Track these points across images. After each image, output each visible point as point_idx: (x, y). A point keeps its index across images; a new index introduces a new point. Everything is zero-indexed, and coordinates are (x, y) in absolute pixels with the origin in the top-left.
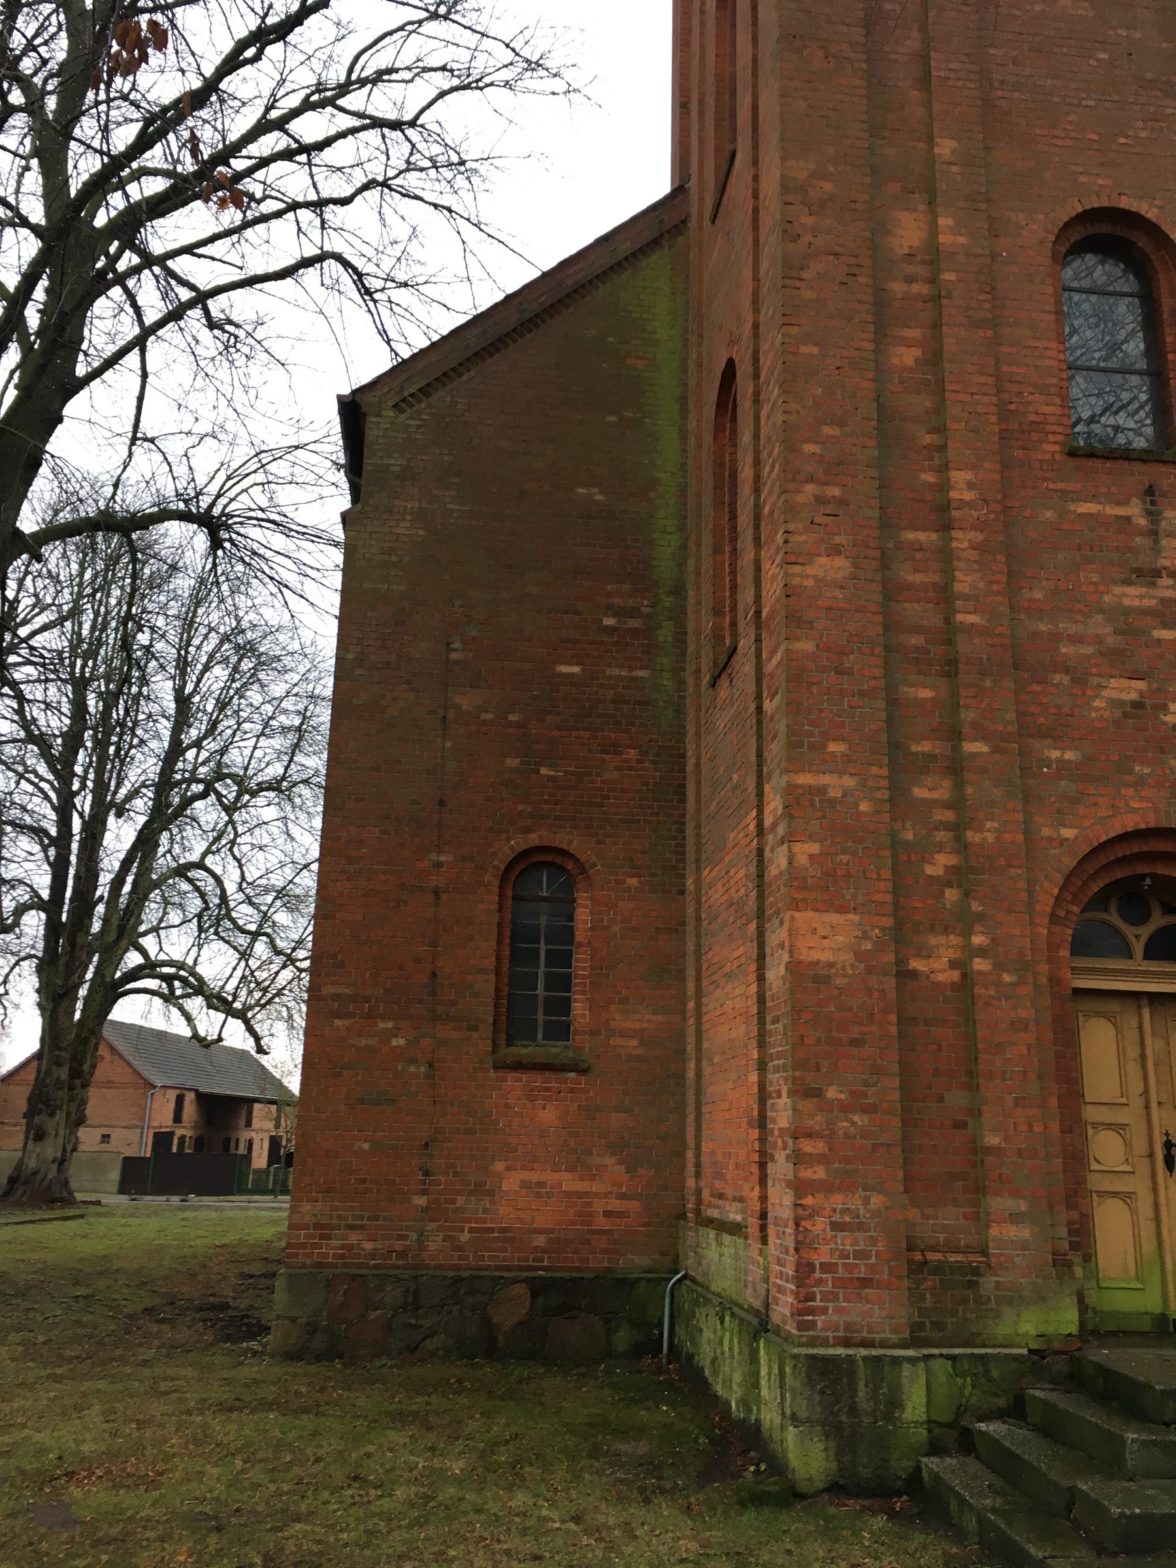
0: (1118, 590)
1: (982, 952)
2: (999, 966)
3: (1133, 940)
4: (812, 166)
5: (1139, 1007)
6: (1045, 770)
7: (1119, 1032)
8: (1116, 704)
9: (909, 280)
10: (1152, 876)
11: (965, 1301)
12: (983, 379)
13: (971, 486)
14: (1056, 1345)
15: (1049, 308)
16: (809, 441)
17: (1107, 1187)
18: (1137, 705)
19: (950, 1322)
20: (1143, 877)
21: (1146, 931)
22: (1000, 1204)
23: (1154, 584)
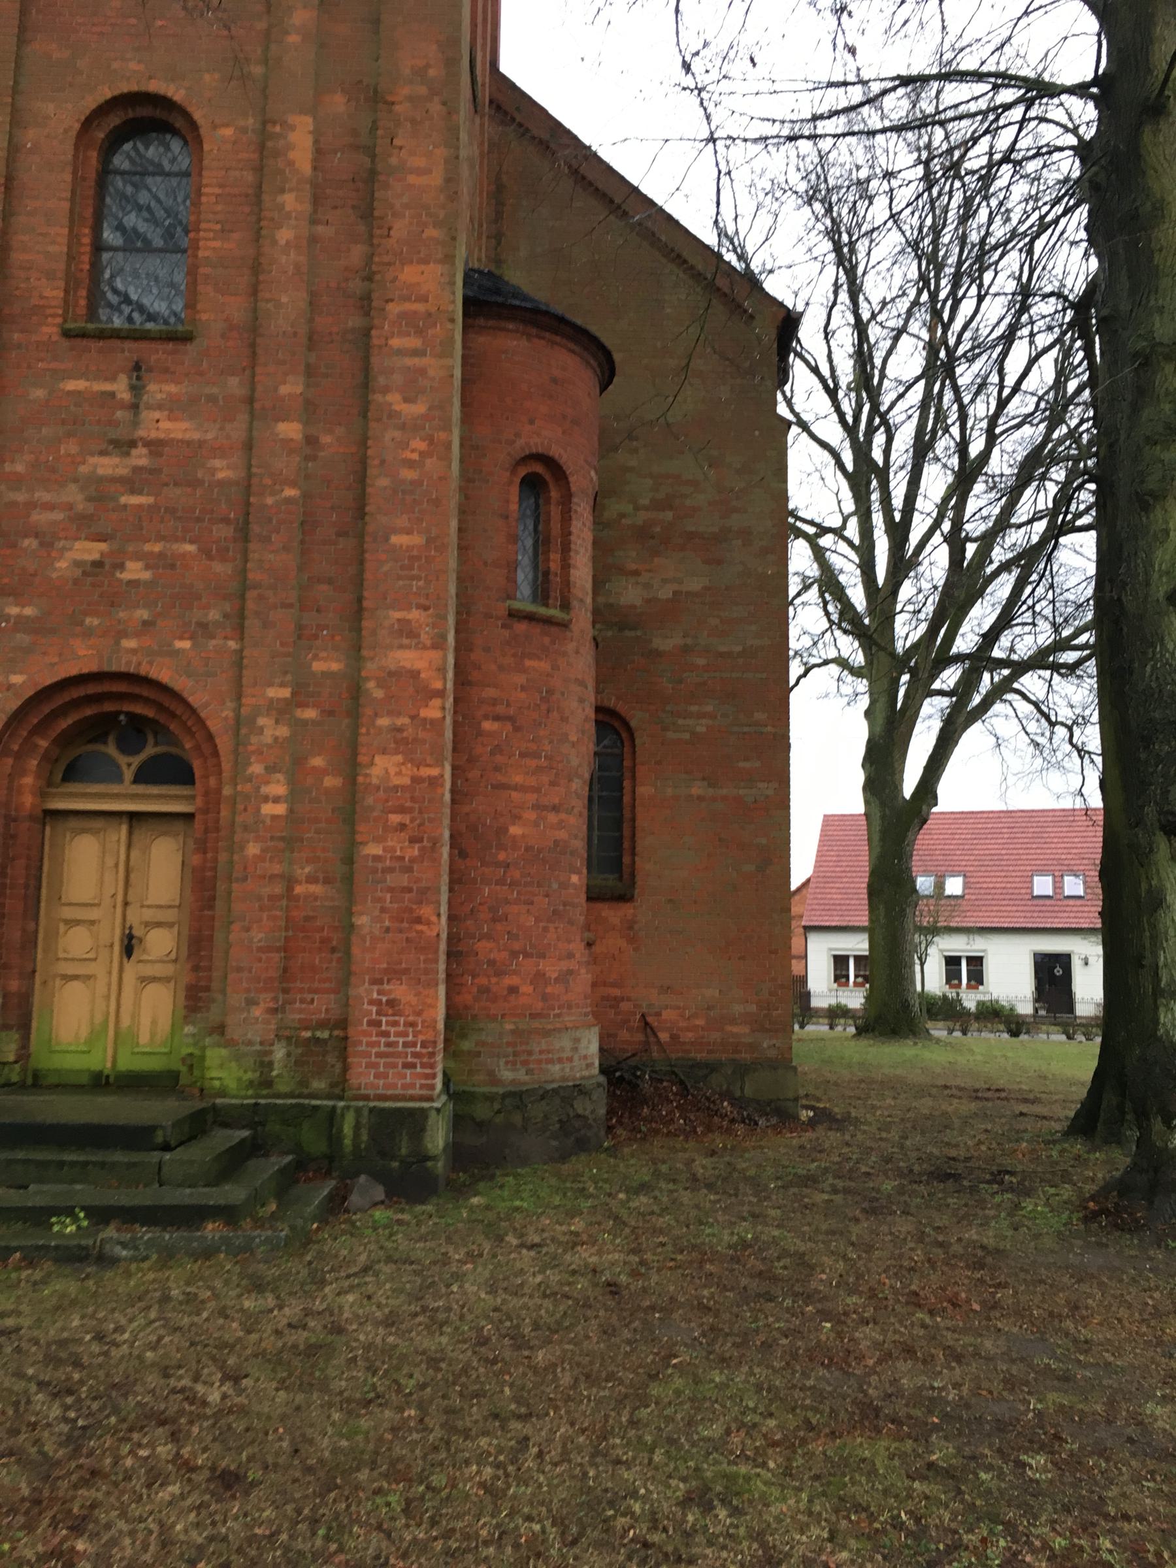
0: (93, 460)
3: (124, 768)
8: (77, 564)
10: (127, 714)
15: (64, 195)
17: (70, 972)
18: (97, 564)
20: (119, 713)
21: (136, 761)
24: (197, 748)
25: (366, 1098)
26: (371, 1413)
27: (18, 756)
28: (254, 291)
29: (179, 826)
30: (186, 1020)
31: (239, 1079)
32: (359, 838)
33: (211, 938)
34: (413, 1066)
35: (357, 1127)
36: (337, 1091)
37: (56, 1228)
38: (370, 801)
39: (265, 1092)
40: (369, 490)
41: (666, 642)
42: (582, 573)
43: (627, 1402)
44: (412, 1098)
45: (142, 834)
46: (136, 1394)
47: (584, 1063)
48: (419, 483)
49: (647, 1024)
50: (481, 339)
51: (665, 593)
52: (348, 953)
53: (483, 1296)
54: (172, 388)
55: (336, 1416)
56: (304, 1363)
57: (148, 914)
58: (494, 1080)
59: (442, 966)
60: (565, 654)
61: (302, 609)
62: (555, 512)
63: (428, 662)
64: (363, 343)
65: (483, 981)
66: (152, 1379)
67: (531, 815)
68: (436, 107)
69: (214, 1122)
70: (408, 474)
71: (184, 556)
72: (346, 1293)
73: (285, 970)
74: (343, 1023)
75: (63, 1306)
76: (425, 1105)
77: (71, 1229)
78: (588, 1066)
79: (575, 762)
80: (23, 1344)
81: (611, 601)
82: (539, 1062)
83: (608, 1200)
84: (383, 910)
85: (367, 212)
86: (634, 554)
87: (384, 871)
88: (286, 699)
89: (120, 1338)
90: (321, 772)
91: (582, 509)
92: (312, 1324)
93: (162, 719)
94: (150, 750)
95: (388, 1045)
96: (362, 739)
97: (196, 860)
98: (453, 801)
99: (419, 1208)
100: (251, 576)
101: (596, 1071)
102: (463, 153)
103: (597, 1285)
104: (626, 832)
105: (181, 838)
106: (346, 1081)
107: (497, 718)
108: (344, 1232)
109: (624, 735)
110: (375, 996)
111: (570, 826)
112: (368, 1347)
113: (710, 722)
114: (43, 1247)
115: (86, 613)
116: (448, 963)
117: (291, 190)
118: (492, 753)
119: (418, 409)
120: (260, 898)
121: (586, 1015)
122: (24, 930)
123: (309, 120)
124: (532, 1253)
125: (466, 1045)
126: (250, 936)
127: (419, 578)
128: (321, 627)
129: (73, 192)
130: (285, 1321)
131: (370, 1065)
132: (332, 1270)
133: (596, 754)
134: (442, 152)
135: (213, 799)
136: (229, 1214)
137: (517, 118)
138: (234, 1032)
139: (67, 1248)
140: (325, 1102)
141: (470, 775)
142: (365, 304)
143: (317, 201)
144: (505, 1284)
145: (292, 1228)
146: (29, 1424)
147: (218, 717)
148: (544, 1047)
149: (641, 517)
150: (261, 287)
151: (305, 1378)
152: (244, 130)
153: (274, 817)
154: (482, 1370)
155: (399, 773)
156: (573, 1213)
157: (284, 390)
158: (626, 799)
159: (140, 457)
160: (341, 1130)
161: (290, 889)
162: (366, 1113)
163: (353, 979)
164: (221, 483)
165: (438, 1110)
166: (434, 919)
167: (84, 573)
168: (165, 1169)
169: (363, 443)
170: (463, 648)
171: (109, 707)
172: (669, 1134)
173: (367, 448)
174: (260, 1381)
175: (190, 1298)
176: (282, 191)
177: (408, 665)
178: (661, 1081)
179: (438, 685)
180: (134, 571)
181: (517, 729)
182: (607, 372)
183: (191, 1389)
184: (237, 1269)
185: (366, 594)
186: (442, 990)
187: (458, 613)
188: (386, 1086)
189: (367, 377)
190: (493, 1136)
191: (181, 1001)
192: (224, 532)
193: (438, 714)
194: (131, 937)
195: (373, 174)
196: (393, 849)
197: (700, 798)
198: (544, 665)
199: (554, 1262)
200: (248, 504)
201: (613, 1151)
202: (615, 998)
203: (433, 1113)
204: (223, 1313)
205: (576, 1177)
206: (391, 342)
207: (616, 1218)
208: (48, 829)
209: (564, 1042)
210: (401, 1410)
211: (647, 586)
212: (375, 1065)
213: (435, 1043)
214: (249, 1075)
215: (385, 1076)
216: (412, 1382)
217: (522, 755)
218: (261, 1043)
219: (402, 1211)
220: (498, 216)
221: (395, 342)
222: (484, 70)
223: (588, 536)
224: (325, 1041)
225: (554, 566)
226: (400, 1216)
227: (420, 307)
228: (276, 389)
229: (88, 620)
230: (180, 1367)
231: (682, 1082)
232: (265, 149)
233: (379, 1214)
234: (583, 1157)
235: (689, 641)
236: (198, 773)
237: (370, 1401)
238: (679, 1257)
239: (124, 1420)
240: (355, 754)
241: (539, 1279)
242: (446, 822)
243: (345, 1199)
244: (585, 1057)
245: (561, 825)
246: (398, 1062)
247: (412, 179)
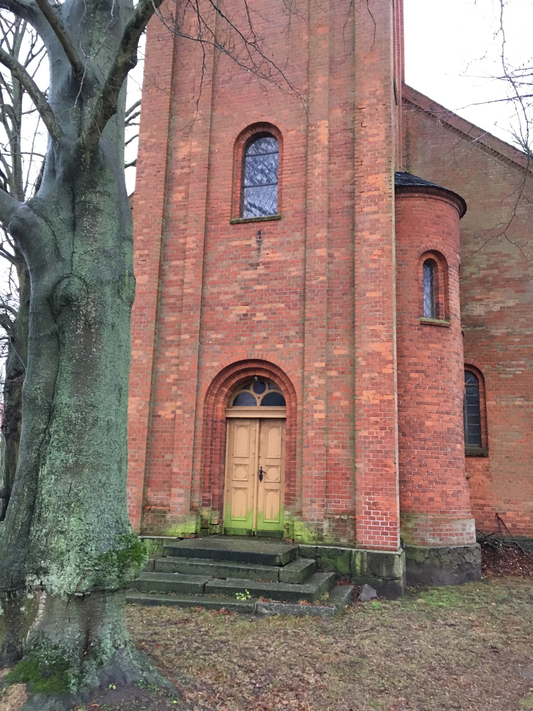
0: (243, 273)
1: (179, 408)
2: (185, 412)
3: (257, 399)
4: (149, 134)
8: (238, 315)
9: (182, 168)
10: (258, 376)
11: (161, 521)
12: (201, 201)
13: (194, 242)
14: (187, 536)
16: (139, 235)
19: (155, 527)
21: (262, 396)
22: (176, 491)
23: (256, 269)
24: (287, 389)
25: (365, 548)
26: (383, 697)
27: (216, 395)
28: (305, 196)
29: (279, 423)
30: (285, 508)
31: (309, 536)
32: (357, 428)
33: (295, 473)
34: (386, 534)
35: (362, 561)
36: (352, 544)
37: (238, 598)
38: (361, 411)
39: (320, 542)
40: (356, 274)
41: (498, 331)
42: (455, 302)
43: (509, 706)
44: (387, 549)
45: (265, 427)
46: (279, 675)
47: (468, 536)
48: (378, 269)
49: (499, 518)
50: (403, 203)
51: (496, 308)
52: (354, 480)
53: (430, 647)
54: (273, 240)
55: (368, 696)
56: (351, 668)
57: (269, 462)
58: (425, 543)
59: (397, 488)
60: (449, 340)
61: (328, 328)
62: (440, 275)
63: (388, 349)
64: (352, 212)
65: (417, 494)
66: (285, 669)
67: (435, 416)
68: (380, 107)
69: (299, 555)
70: (373, 266)
71: (279, 309)
72: (365, 639)
73: (327, 487)
74: (353, 513)
75: (245, 633)
76: (394, 553)
77: (244, 599)
78: (471, 538)
79: (456, 391)
80: (231, 648)
81: (468, 314)
82: (446, 535)
83: (487, 605)
84: (369, 461)
85: (352, 157)
86: (479, 291)
87: (369, 443)
88: (323, 367)
89: (269, 649)
90: (339, 399)
91: (453, 273)
92: (351, 652)
94: (267, 391)
95: (374, 523)
96: (357, 384)
97: (287, 438)
98: (399, 411)
99: (393, 602)
100: (306, 315)
101: (475, 540)
102: (393, 125)
103: (486, 647)
104: (482, 423)
105: (280, 429)
106: (356, 539)
107: (417, 372)
108: (360, 611)
109: (479, 377)
110: (367, 500)
111: (456, 421)
112: (378, 666)
113: (523, 369)
114: (233, 605)
115: (241, 335)
116: (400, 486)
117: (319, 152)
118: (416, 387)
119: (376, 237)
120: (315, 455)
121: (468, 512)
122: (220, 468)
123: (327, 122)
124: (451, 629)
125: (410, 525)
126: (311, 472)
127: (379, 311)
128: (337, 335)
129: (233, 167)
130: (339, 649)
131: (367, 533)
132: (357, 628)
133: (466, 386)
134: (384, 126)
135: (294, 412)
136: (309, 597)
137: (415, 105)
138: (306, 515)
139: (243, 607)
140: (347, 549)
141: (405, 398)
142: (352, 195)
143: (330, 155)
144: (440, 642)
145: (337, 606)
146: (237, 684)
147: (294, 375)
148: (448, 528)
149: (482, 273)
150: (308, 194)
151: (351, 677)
152: (300, 131)
153: (320, 419)
154: (433, 682)
155: (374, 399)
156: (469, 611)
157: (318, 235)
158: (482, 407)
159: (261, 270)
160: (355, 562)
161: (327, 451)
162: (365, 554)
163: (357, 492)
164: (294, 277)
165: (399, 555)
166: (393, 465)
167: (241, 319)
168: (281, 575)
169: (353, 254)
170: (400, 339)
171: (251, 374)
172: (514, 574)
173: (355, 256)
174: (331, 676)
175: (296, 634)
176: (316, 153)
177: (376, 350)
178: (508, 547)
179: (390, 358)
180: (260, 316)
181: (427, 376)
182: (462, 208)
183: (302, 676)
184: (314, 623)
185: (356, 319)
186: (398, 498)
187: (397, 325)
188: (375, 543)
189: (353, 226)
190: (424, 570)
191: (283, 500)
192: (294, 297)
193: (391, 371)
194: (261, 472)
195: (354, 139)
196: (373, 433)
197: (520, 407)
198: (439, 346)
199: (462, 634)
200: (304, 285)
201: (486, 581)
202: (482, 505)
203: (397, 557)
204: (311, 642)
205: (468, 593)
206: (364, 210)
207: (492, 615)
208: (228, 426)
209: (457, 526)
210: (397, 697)
211: (487, 305)
212: (369, 533)
213: (396, 523)
214: (313, 535)
215: (373, 538)
216: (401, 684)
217: (430, 388)
218: (318, 520)
219: (386, 603)
220: (408, 146)
221: (366, 210)
222: (399, 85)
223: (457, 285)
224: (346, 520)
225: (441, 300)
226: (384, 605)
227: (376, 193)
228: (315, 235)
229: (242, 338)
230: (296, 665)
231: (520, 549)
232: (308, 137)
233: (374, 603)
234: (472, 583)
235: (510, 330)
236: (287, 400)
237: (382, 691)
238: (527, 637)
239: (275, 687)
240: (354, 391)
241: (456, 642)
242: (396, 420)
243: (359, 595)
244: (469, 533)
245: (451, 420)
246: (378, 534)
247: (371, 139)
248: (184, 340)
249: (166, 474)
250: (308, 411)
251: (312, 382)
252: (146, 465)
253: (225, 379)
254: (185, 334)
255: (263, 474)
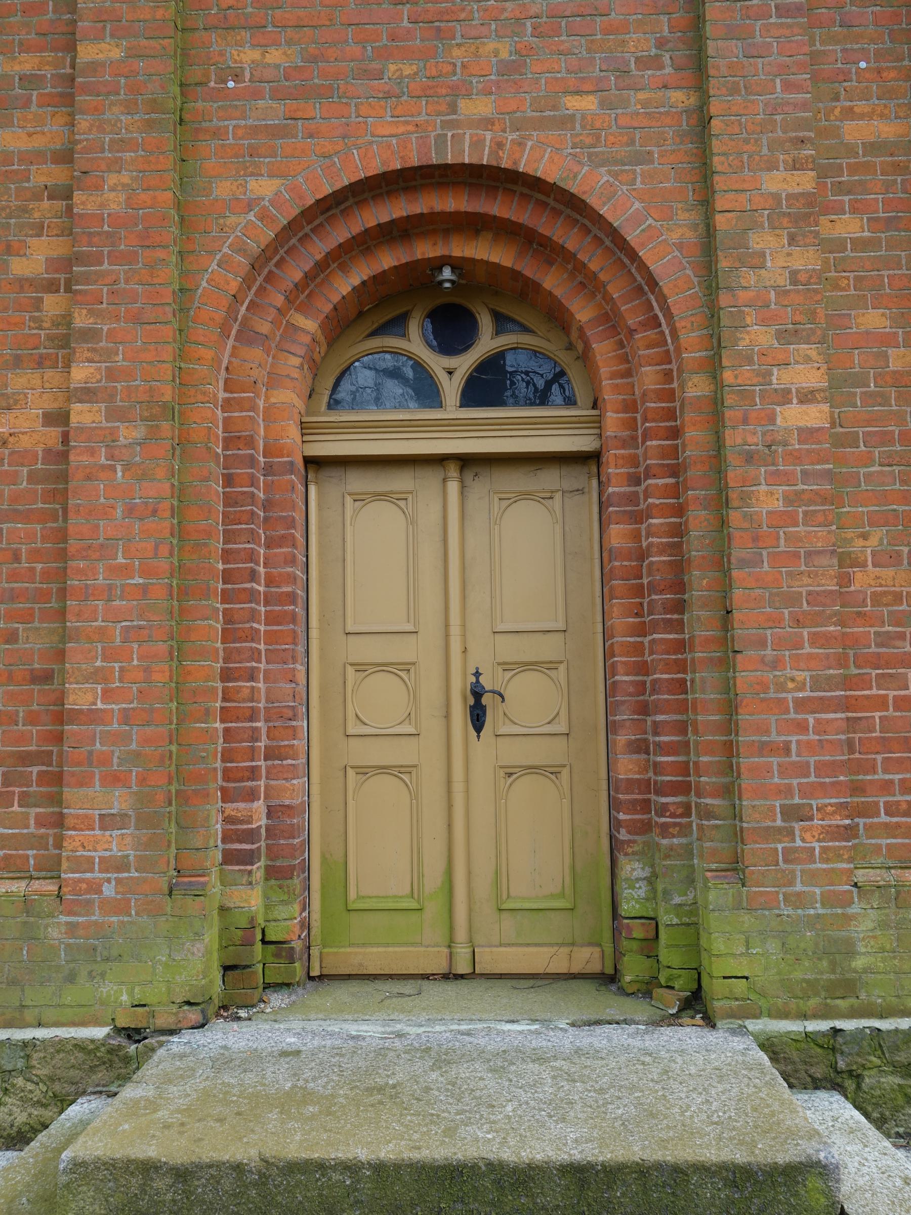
1: (87, 394)
2: (114, 414)
3: (442, 377)
5: (445, 480)
6: (231, 84)
7: (412, 521)
10: (457, 265)
21: (465, 363)
57: (510, 650)
93: (528, 268)
120: (792, 600)
153: (807, 434)
161: (845, 580)
208: (312, 489)
248: (94, 67)
249: (32, 719)
250: (746, 395)
251: (757, 262)
252: (698, 945)
253: (308, 266)
254: (99, 37)
255: (486, 700)
